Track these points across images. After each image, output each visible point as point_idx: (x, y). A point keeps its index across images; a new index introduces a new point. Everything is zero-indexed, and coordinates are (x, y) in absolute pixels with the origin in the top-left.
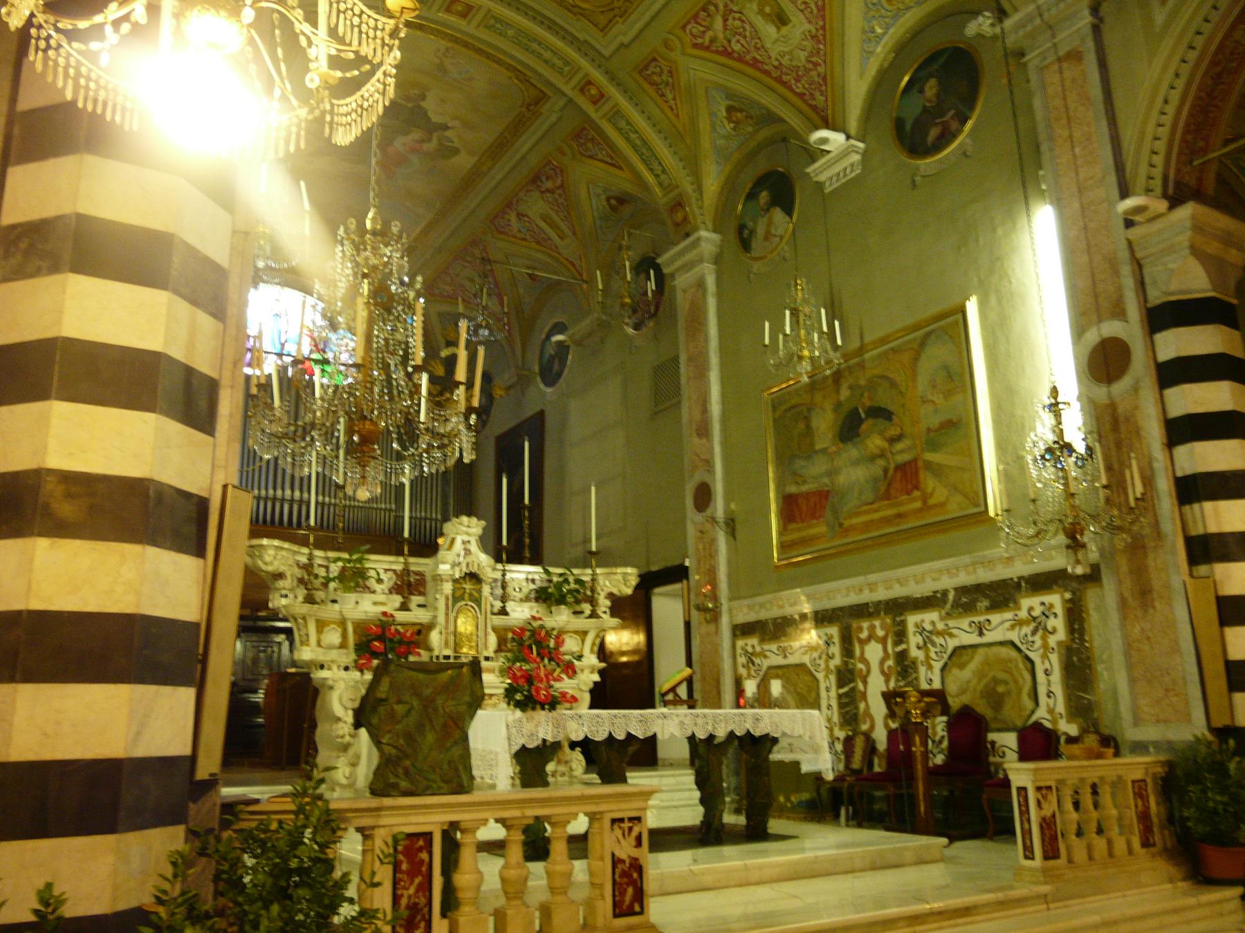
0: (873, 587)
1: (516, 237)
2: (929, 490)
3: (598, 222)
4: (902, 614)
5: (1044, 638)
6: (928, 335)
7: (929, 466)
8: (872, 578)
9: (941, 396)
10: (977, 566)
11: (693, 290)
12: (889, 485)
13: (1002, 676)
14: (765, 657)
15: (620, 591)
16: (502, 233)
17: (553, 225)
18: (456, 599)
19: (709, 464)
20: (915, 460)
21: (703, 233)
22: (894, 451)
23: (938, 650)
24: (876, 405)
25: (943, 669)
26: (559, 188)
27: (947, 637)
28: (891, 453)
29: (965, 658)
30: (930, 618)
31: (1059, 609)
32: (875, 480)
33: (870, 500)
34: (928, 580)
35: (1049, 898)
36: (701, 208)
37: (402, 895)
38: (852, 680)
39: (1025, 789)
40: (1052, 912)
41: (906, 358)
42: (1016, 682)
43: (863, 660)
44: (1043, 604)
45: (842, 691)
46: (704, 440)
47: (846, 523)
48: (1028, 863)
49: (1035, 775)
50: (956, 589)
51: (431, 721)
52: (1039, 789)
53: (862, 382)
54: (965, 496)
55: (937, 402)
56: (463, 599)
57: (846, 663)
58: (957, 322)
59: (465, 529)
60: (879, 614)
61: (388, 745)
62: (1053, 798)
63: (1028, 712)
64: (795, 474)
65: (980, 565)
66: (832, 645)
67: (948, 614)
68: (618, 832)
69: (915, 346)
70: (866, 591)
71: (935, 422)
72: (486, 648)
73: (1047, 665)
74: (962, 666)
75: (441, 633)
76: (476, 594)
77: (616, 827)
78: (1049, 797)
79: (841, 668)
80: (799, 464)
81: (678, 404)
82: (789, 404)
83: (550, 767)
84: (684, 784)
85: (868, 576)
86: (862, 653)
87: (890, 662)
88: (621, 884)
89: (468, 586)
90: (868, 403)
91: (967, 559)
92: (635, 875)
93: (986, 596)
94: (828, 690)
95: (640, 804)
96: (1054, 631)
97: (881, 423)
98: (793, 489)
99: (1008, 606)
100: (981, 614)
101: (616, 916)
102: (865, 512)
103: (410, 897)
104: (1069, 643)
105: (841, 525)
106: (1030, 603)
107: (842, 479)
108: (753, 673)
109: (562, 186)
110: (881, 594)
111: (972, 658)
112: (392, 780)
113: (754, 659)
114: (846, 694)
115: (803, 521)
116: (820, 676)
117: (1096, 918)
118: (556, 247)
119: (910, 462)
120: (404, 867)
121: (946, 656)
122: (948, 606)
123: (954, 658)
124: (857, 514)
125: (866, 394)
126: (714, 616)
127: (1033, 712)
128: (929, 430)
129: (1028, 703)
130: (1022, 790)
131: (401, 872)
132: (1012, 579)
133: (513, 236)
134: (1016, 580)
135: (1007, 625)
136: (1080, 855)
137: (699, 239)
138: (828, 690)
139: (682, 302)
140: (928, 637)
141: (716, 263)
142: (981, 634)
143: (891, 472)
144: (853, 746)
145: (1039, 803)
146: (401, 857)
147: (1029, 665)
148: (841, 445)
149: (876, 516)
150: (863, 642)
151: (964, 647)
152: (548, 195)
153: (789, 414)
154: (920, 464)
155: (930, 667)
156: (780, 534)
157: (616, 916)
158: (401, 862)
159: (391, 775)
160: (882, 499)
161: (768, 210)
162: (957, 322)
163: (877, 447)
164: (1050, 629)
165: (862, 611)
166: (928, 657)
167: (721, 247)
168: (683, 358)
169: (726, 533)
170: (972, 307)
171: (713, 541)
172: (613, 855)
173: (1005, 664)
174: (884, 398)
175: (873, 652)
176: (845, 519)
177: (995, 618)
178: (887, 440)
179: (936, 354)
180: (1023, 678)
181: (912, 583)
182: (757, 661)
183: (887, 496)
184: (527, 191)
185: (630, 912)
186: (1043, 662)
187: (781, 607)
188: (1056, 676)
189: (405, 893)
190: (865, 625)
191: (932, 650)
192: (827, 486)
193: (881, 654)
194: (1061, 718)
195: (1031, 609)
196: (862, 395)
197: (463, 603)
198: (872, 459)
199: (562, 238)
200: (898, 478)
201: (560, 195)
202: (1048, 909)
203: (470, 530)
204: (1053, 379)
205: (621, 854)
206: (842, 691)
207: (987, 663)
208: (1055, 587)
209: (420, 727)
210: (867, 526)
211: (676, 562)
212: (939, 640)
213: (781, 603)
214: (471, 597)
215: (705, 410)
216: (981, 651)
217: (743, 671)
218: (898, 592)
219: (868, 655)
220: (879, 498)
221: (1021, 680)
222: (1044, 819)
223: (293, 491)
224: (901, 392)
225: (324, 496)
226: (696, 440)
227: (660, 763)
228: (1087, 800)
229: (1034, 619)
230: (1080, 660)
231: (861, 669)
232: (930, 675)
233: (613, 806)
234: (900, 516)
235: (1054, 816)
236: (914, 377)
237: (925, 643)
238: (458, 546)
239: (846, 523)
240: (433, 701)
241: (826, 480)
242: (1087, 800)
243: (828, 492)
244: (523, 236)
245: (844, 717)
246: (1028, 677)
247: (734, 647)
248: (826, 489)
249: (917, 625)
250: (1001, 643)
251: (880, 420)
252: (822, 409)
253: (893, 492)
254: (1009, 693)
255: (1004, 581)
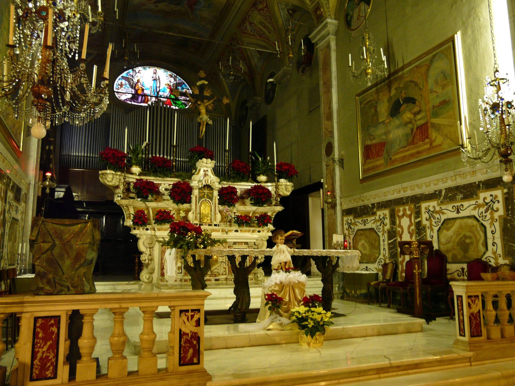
0: (405, 189)
1: (250, 34)
2: (433, 138)
3: (284, 23)
4: (419, 203)
5: (491, 214)
6: (434, 56)
7: (433, 125)
8: (405, 185)
9: (440, 88)
10: (457, 176)
11: (325, 49)
12: (414, 137)
13: (468, 234)
14: (356, 225)
15: (284, 193)
16: (245, 33)
17: (265, 27)
18: (200, 198)
19: (332, 133)
20: (427, 123)
21: (329, 20)
22: (416, 119)
23: (436, 221)
24: (408, 96)
25: (438, 231)
26: (265, 8)
27: (441, 214)
28: (415, 121)
29: (450, 225)
30: (433, 204)
31: (500, 198)
32: (407, 135)
33: (405, 145)
34: (432, 185)
35: (472, 360)
36: (328, 8)
37: (38, 352)
38: (395, 236)
39: (461, 297)
40: (473, 367)
41: (423, 70)
42: (476, 237)
43: (400, 226)
44: (491, 195)
45: (390, 242)
46: (330, 122)
47: (393, 158)
48: (462, 338)
49: (467, 289)
50: (445, 189)
51: (68, 253)
52: (469, 297)
53: (402, 85)
54: (452, 140)
55: (438, 91)
56: (204, 198)
57: (392, 228)
58: (449, 47)
59: (205, 165)
60: (408, 203)
61: (38, 265)
62: (479, 303)
63: (482, 253)
64: (370, 135)
65: (458, 176)
66: (386, 219)
67: (441, 202)
68: (184, 318)
69: (428, 63)
70: (402, 192)
71: (437, 102)
72: (215, 220)
73: (493, 228)
74: (448, 229)
75: (193, 213)
76: (210, 195)
77: (183, 315)
78: (477, 301)
79: (390, 230)
80: (372, 130)
81: (319, 106)
82: (368, 100)
83: (207, 278)
84: (318, 284)
85: (403, 184)
86: (400, 223)
87: (413, 227)
88: (184, 347)
89: (206, 191)
90: (404, 96)
91: (451, 173)
92: (195, 342)
93: (461, 193)
94: (384, 241)
95: (200, 302)
96: (497, 210)
97: (410, 105)
98: (369, 143)
99: (472, 197)
100: (459, 202)
101: (180, 365)
102: (402, 152)
103: (43, 352)
104: (506, 216)
105: (391, 159)
106: (485, 195)
107: (391, 136)
108: (351, 232)
109: (267, 6)
110: (409, 193)
111: (454, 225)
112: (41, 286)
113: (351, 226)
114: (392, 243)
115: (373, 158)
116: (380, 234)
117: (498, 374)
118: (268, 37)
119: (424, 124)
120: (40, 335)
121: (440, 224)
122: (442, 198)
123: (444, 225)
124: (398, 153)
125: (403, 91)
126: (333, 206)
127: (484, 253)
128: (434, 106)
129: (482, 249)
130: (460, 297)
131: (38, 338)
132: (475, 183)
133: (248, 34)
134: (477, 183)
135: (472, 207)
136: (495, 333)
137: (327, 23)
138: (384, 241)
139: (321, 56)
140: (431, 214)
141: (336, 35)
142: (458, 212)
143: (415, 130)
144: (387, 268)
145: (469, 305)
146: (38, 330)
147: (483, 229)
148: (391, 119)
149: (407, 153)
150: (400, 217)
151: (449, 219)
152: (261, 12)
153: (367, 106)
154: (429, 125)
155: (432, 230)
156: (363, 165)
157: (180, 365)
158: (39, 333)
159: (40, 283)
160: (410, 145)
161: (359, 4)
162: (449, 47)
163: (408, 118)
164: (495, 209)
165: (400, 202)
166: (431, 224)
167: (338, 27)
168: (321, 83)
169: (339, 165)
170: (458, 38)
171: (334, 170)
172: (180, 330)
173: (471, 228)
174: (412, 93)
175: (405, 222)
176: (392, 156)
177: (466, 204)
178: (413, 114)
179: (439, 65)
180: (480, 235)
181: (424, 187)
182: (352, 227)
183: (413, 143)
184: (252, 11)
185: (191, 363)
186: (491, 227)
187: (363, 201)
188: (498, 234)
189: (41, 350)
190: (401, 209)
191: (434, 221)
192: (384, 140)
193: (408, 223)
194: (500, 257)
195: (485, 199)
196: (401, 92)
197: (204, 199)
198: (406, 124)
199: (270, 33)
200: (418, 133)
201: (266, 11)
202: (471, 365)
203: (208, 165)
204: (496, 66)
205: (185, 330)
206: (390, 242)
207: (461, 227)
208: (499, 186)
209: (61, 256)
210: (403, 158)
211: (319, 181)
212: (437, 216)
213: (363, 199)
214: (208, 197)
215: (330, 108)
216: (458, 221)
217: (346, 232)
218: (417, 191)
219: (402, 224)
220: (409, 144)
221: (478, 237)
222: (472, 314)
223: (170, 157)
224: (420, 88)
225: (181, 158)
226: (327, 122)
227: (312, 274)
228: (503, 304)
229: (487, 204)
230: (511, 225)
231: (399, 231)
232: (432, 234)
233: (181, 303)
234: (419, 153)
235: (479, 312)
236: (427, 81)
237: (430, 217)
238: (202, 172)
239: (393, 158)
240: (69, 241)
241: (384, 137)
242: (503, 304)
243: (385, 142)
244: (253, 33)
245: (391, 254)
246: (482, 235)
247: (342, 220)
248: (384, 141)
249: (426, 208)
250: (469, 217)
251: (410, 104)
252: (383, 101)
253: (415, 140)
254: (472, 243)
255: (471, 184)
